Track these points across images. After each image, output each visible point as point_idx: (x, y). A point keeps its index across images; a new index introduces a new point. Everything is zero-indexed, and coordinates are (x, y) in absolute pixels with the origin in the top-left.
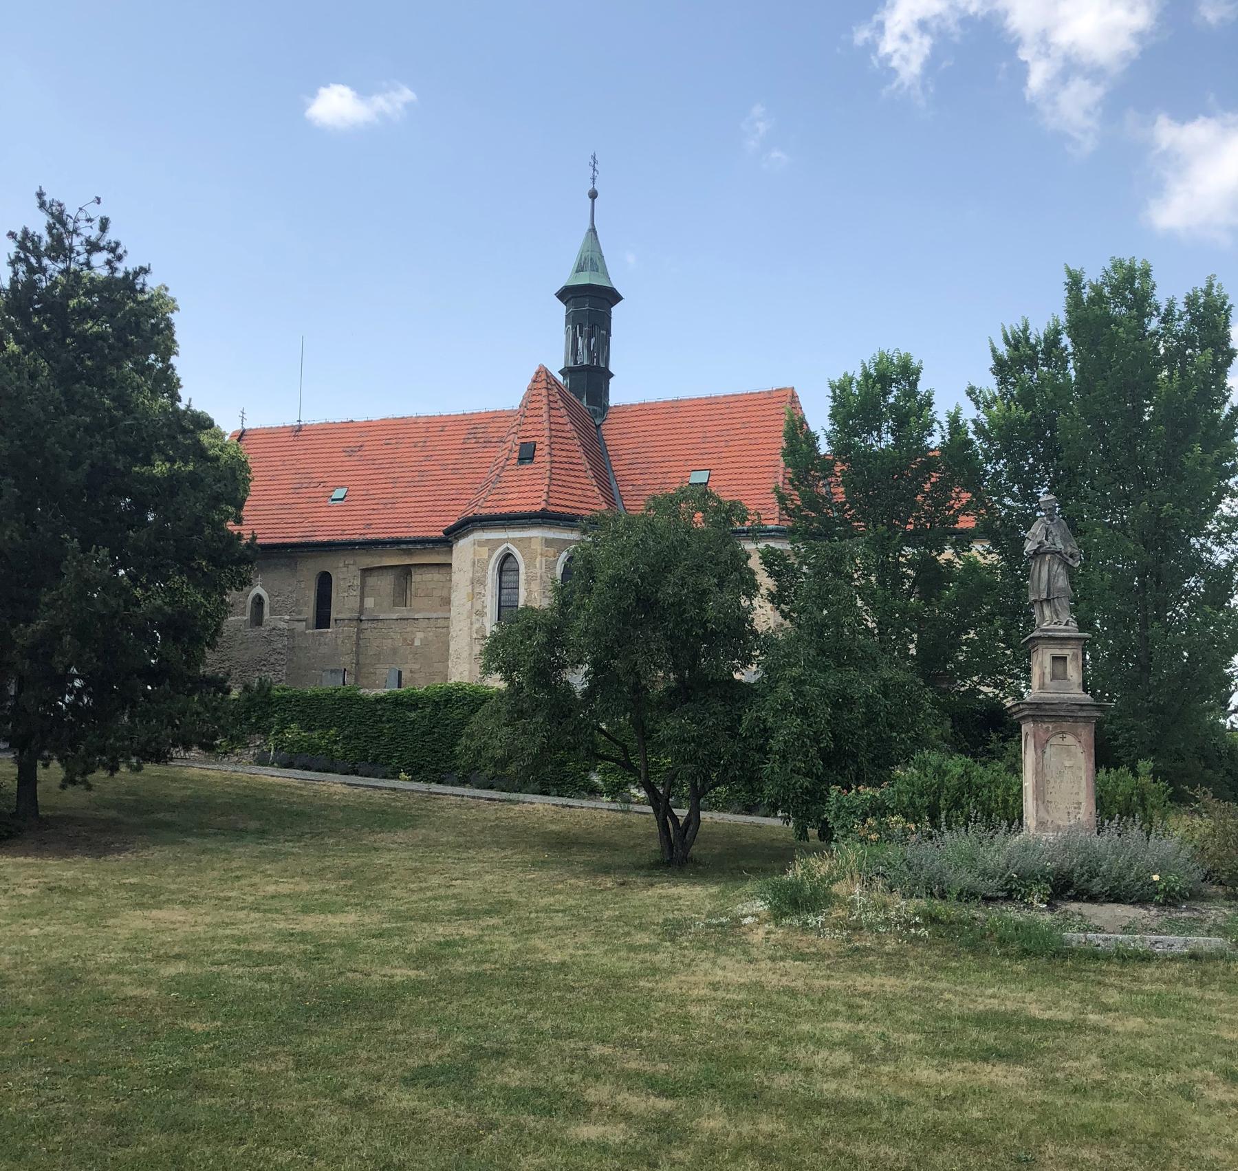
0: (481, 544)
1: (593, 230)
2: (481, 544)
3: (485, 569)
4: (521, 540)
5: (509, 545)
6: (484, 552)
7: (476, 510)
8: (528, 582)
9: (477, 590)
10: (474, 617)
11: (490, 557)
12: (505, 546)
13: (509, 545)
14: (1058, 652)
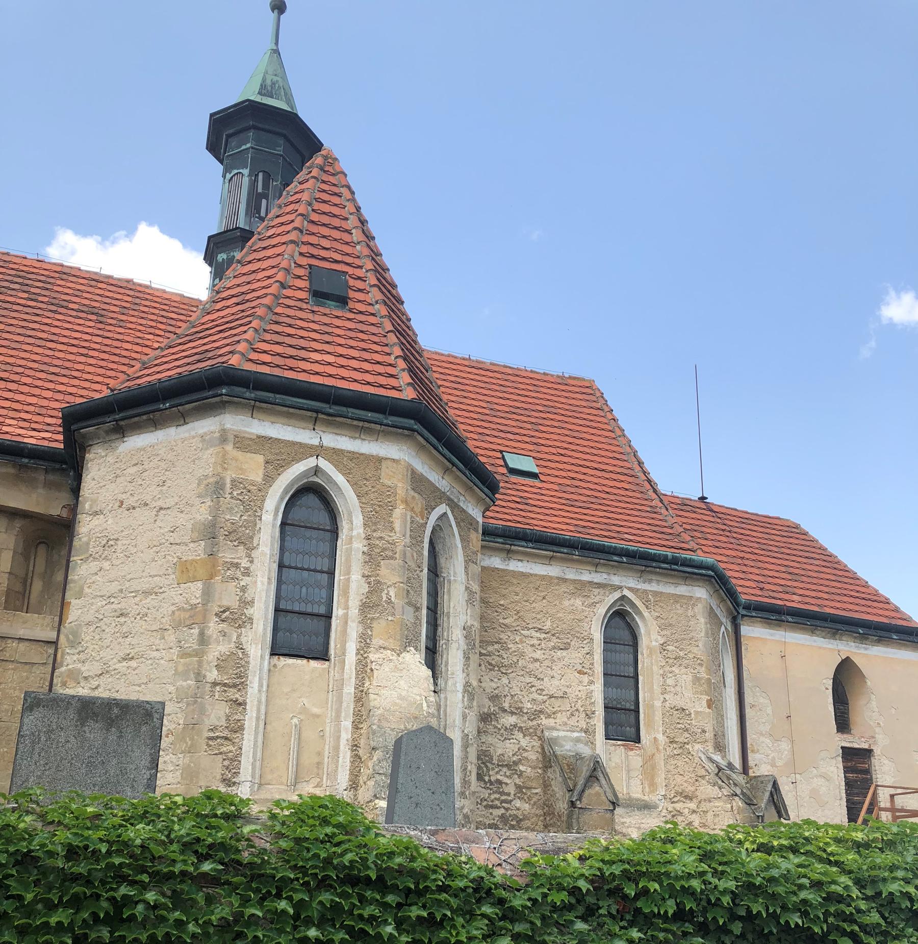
0: (244, 443)
1: (276, 52)
2: (244, 443)
3: (252, 503)
4: (354, 456)
5: (324, 464)
6: (253, 467)
7: (234, 360)
8: (372, 558)
9: (226, 555)
10: (213, 627)
11: (269, 479)
12: (311, 462)
13: (324, 464)
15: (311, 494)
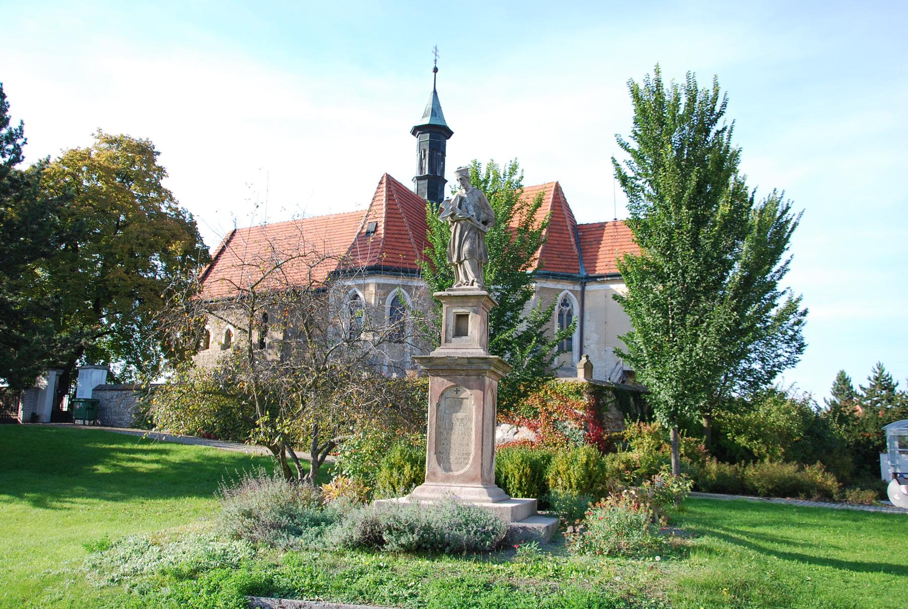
1: (435, 92)
14: (461, 311)
15: (396, 300)
